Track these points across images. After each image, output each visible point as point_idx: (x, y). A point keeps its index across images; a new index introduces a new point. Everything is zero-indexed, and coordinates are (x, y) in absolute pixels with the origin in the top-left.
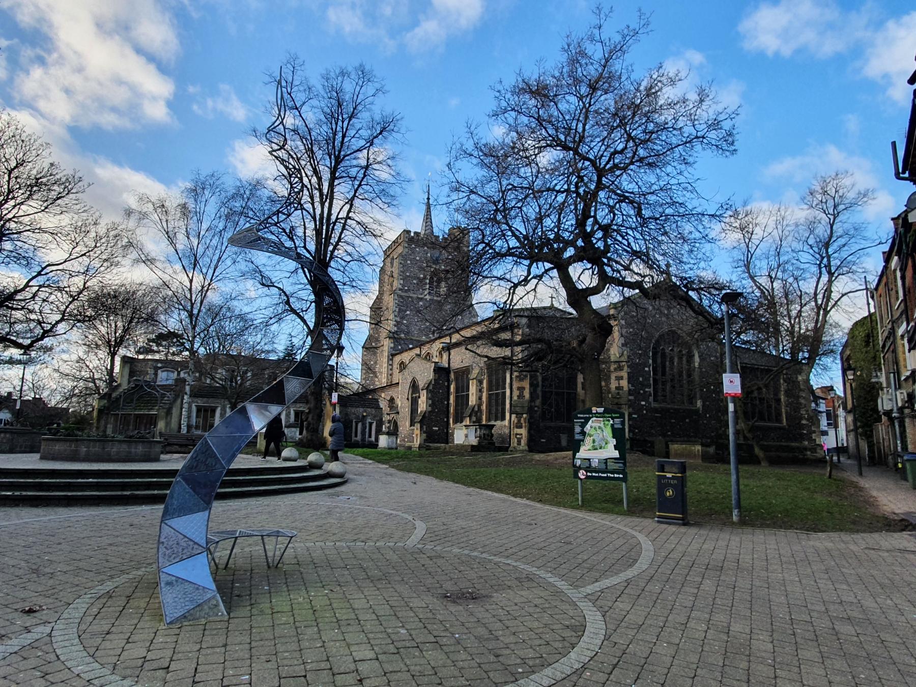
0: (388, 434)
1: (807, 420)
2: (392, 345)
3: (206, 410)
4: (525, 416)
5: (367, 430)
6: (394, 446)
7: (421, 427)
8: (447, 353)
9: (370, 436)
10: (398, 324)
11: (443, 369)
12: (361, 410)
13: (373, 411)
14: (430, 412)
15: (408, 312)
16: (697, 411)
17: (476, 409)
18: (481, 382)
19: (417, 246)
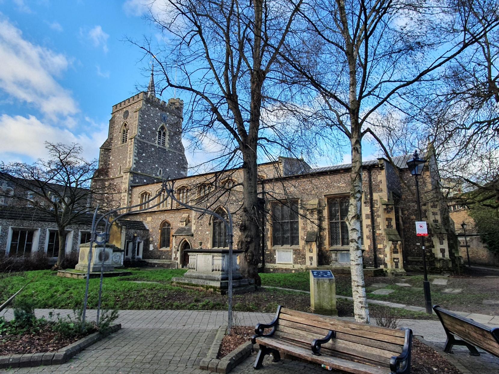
2: (132, 179)
3: (23, 233)
4: (399, 242)
5: (136, 248)
10: (137, 163)
13: (142, 232)
15: (144, 155)
18: (320, 212)
19: (152, 105)
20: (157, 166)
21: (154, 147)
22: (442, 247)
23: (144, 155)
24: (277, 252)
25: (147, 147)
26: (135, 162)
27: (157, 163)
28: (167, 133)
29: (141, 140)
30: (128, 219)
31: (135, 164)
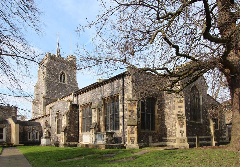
0: (46, 138)
1: (224, 127)
6: (49, 144)
8: (77, 97)
9: (37, 138)
11: (75, 105)
12: (31, 127)
14: (69, 127)
16: (201, 124)
17: (98, 124)
18: (100, 110)
20: (60, 94)
21: (58, 83)
22: (182, 129)
23: (52, 88)
24: (83, 135)
25: (53, 84)
26: (46, 92)
27: (61, 92)
28: (66, 76)
29: (49, 80)
30: (36, 121)
31: (46, 93)
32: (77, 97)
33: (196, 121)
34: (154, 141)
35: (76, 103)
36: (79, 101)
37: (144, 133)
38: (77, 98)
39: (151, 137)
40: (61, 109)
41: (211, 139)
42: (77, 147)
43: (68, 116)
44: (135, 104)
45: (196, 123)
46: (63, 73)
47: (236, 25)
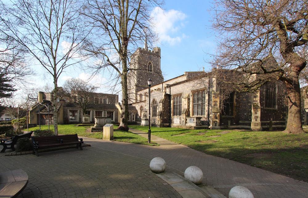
7: (160, 117)
8: (169, 88)
9: (133, 120)
14: (163, 111)
16: (276, 110)
17: (187, 110)
22: (257, 115)
28: (152, 65)
32: (169, 88)
33: (271, 107)
34: (232, 124)
35: (169, 93)
36: (171, 92)
37: (224, 118)
38: (169, 90)
39: (230, 121)
40: (156, 98)
41: (286, 123)
42: (46, 125)
43: (163, 103)
44: (218, 96)
45: (270, 110)
46: (150, 63)
47: (224, 176)
